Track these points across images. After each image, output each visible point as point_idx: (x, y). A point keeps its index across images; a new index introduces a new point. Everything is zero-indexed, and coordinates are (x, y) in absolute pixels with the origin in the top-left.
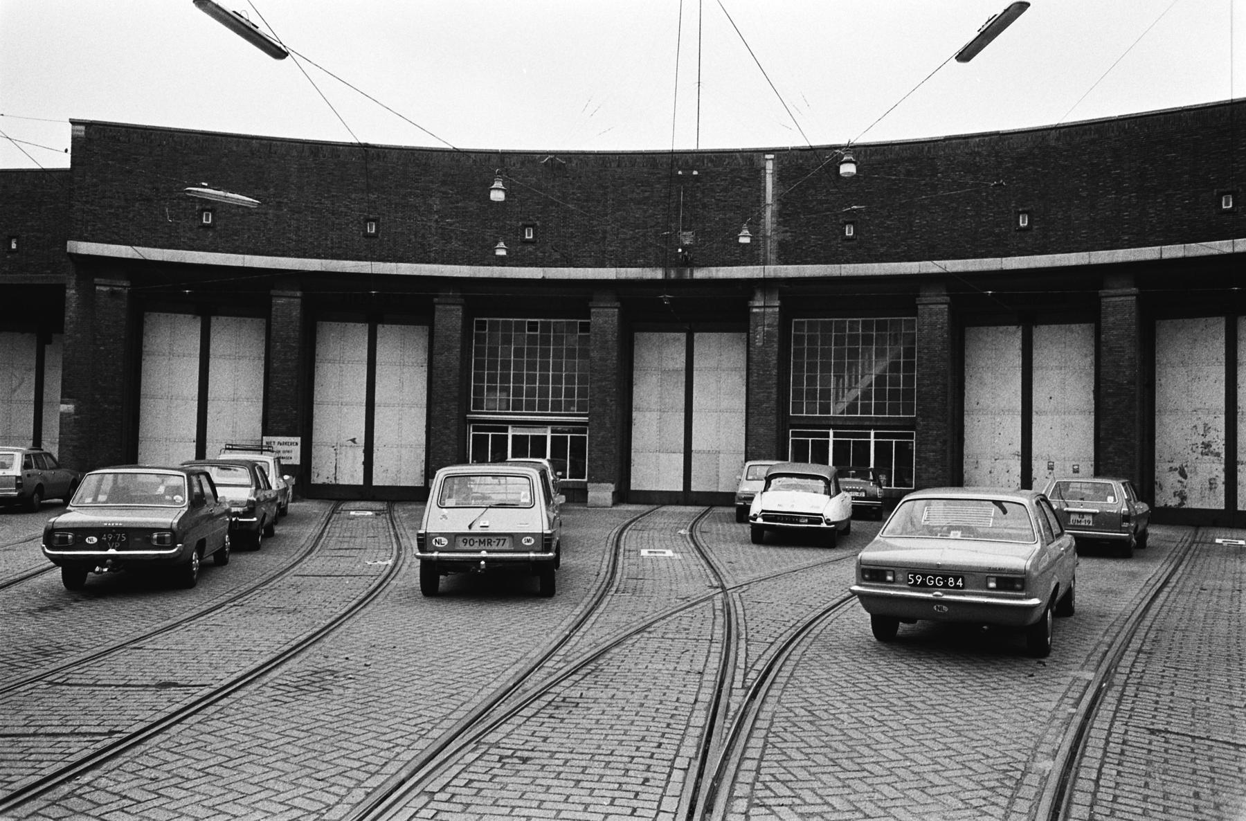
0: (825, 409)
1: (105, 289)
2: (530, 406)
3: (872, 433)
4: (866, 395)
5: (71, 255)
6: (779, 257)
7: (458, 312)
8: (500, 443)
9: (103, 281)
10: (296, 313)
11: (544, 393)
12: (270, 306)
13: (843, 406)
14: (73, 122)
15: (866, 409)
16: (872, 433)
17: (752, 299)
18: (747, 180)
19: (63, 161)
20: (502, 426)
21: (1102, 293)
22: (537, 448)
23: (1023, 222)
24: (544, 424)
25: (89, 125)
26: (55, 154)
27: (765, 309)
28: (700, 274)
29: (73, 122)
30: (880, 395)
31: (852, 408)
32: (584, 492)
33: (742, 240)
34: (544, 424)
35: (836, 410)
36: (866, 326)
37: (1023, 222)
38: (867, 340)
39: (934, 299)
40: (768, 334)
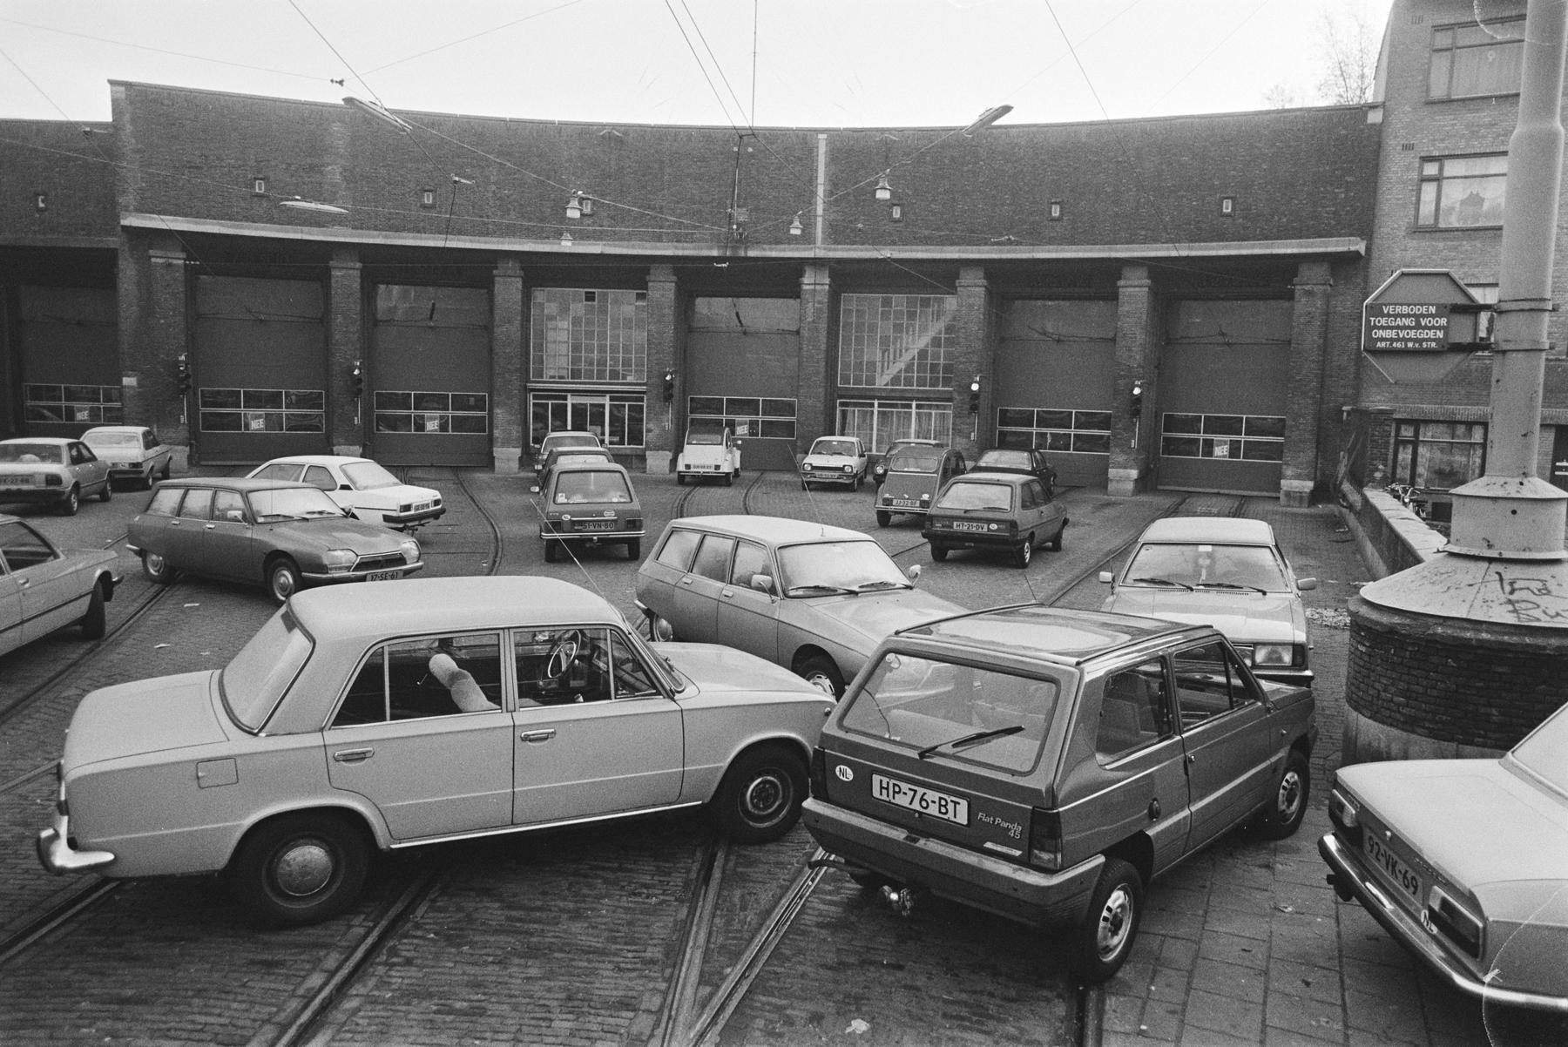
0: (871, 380)
1: (160, 261)
2: (589, 374)
3: (914, 404)
4: (909, 368)
5: (124, 227)
6: (839, 150)
7: (518, 284)
8: (560, 412)
9: (159, 253)
10: (356, 285)
11: (602, 363)
12: (330, 277)
13: (887, 378)
14: (112, 83)
15: (908, 382)
16: (914, 404)
17: (802, 276)
18: (800, 159)
19: (106, 116)
20: (561, 395)
21: (1121, 283)
22: (598, 419)
23: (1056, 211)
24: (604, 393)
25: (128, 85)
26: (99, 111)
27: (815, 283)
28: (751, 254)
29: (112, 83)
30: (921, 368)
31: (895, 380)
32: (643, 458)
33: (793, 232)
34: (604, 393)
35: (882, 382)
36: (910, 303)
37: (1056, 211)
38: (912, 315)
39: (970, 282)
40: (818, 311)
